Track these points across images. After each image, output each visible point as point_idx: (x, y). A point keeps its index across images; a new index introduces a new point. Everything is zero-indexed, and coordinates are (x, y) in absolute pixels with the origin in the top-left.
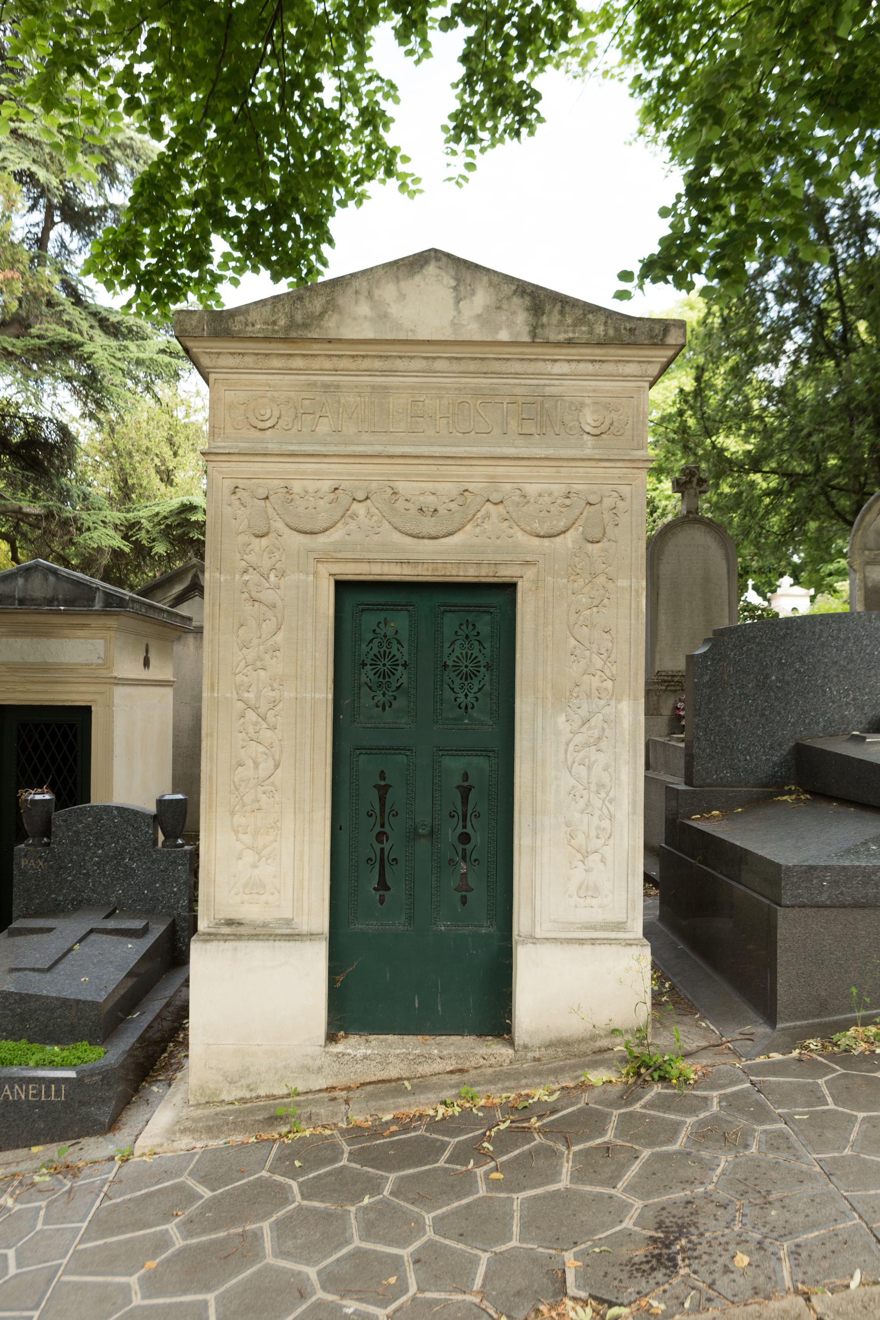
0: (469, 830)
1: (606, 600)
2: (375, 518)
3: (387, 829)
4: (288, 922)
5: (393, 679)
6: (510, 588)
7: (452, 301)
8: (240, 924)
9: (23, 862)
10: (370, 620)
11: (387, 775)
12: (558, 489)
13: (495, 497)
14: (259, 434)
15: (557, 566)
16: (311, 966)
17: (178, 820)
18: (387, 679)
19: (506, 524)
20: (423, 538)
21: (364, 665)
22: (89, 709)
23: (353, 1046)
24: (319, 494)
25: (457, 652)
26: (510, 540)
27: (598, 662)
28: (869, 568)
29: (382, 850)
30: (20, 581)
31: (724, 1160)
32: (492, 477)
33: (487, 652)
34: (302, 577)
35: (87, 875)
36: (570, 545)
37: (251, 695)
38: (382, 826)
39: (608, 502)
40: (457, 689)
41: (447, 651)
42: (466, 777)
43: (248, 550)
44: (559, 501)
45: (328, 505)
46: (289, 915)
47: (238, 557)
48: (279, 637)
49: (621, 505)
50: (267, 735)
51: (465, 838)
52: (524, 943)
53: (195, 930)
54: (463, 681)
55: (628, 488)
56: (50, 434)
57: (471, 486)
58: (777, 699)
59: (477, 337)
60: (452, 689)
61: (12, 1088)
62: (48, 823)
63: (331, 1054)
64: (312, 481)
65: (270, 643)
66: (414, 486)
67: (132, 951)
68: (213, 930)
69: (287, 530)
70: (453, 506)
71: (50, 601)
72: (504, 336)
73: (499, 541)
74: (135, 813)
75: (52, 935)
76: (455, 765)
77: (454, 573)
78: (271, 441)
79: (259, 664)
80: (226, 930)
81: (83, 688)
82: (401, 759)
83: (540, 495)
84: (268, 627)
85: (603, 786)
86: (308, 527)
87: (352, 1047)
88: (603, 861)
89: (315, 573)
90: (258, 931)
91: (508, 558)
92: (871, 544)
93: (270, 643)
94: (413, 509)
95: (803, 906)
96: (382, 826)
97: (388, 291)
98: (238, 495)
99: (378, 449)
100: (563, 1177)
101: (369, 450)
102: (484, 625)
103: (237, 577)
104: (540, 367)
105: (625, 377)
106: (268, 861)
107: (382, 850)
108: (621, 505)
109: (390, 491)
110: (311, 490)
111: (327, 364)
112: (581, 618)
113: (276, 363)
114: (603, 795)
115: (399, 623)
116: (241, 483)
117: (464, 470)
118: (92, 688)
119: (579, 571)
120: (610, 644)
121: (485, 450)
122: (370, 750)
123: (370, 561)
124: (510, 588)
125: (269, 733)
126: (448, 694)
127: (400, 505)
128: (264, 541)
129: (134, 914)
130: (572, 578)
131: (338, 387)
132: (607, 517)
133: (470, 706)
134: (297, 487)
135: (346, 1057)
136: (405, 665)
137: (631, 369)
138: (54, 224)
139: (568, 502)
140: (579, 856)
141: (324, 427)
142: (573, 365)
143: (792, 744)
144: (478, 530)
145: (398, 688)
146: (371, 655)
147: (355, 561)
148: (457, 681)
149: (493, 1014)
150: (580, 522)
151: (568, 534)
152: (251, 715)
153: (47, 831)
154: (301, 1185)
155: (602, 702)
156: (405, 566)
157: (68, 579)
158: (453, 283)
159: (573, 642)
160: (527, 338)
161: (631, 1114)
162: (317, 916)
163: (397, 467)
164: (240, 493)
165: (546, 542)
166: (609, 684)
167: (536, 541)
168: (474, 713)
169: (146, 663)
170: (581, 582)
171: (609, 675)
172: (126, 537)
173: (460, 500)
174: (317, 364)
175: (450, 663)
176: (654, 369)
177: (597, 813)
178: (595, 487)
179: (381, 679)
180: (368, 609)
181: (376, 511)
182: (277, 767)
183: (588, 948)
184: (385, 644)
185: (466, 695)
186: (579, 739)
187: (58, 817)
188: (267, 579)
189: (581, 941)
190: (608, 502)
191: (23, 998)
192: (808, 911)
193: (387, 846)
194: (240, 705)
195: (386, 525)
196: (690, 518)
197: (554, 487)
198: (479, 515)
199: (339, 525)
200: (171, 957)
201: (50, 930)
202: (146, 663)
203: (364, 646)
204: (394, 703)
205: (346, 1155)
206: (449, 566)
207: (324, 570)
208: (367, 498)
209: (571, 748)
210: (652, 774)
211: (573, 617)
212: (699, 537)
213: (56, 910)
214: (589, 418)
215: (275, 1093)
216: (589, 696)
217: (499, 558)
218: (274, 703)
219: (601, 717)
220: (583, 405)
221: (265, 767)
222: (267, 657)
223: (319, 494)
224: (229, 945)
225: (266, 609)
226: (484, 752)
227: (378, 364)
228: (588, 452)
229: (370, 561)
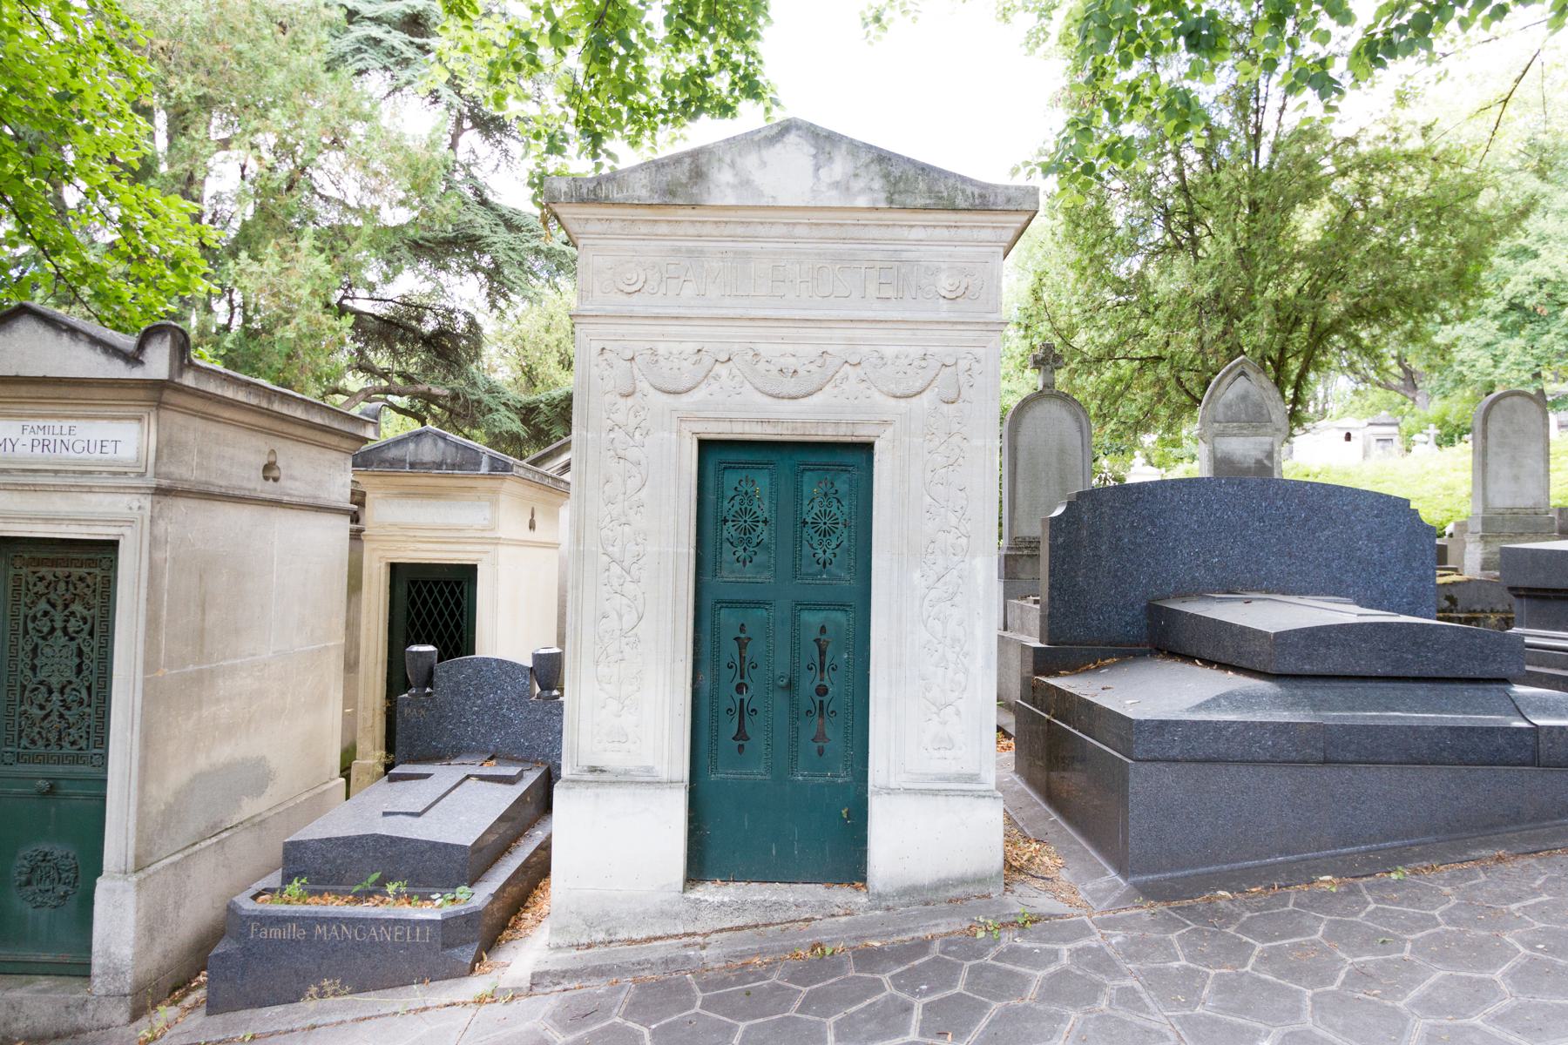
0: (826, 682)
3: (747, 680)
4: (649, 770)
6: (867, 448)
7: (810, 169)
9: (406, 711)
10: (731, 479)
11: (747, 628)
14: (625, 297)
16: (667, 820)
17: (548, 671)
19: (864, 385)
21: (725, 521)
22: (475, 567)
23: (710, 893)
25: (816, 510)
28: (1218, 439)
29: (742, 701)
31: (1074, 1016)
32: (850, 339)
33: (845, 509)
34: (666, 435)
35: (467, 723)
38: (742, 677)
39: (963, 365)
41: (806, 508)
42: (823, 630)
47: (605, 415)
48: (643, 494)
49: (976, 366)
50: (630, 588)
51: (822, 691)
52: (878, 793)
53: (559, 777)
56: (461, 325)
57: (830, 349)
58: (1129, 560)
59: (834, 204)
61: (339, 928)
62: (431, 673)
63: (688, 900)
64: (676, 344)
65: (635, 498)
66: (777, 349)
67: (506, 796)
69: (652, 390)
70: (812, 367)
71: (439, 466)
72: (862, 202)
74: (513, 665)
75: (428, 781)
76: (812, 619)
78: (638, 304)
79: (623, 520)
80: (589, 777)
81: (469, 548)
82: (761, 613)
87: (711, 894)
88: (958, 713)
89: (679, 431)
90: (620, 778)
91: (865, 417)
92: (1220, 417)
93: (635, 498)
94: (774, 371)
95: (1155, 760)
96: (742, 677)
97: (750, 161)
99: (739, 312)
100: (912, 1030)
101: (731, 313)
102: (842, 486)
104: (898, 233)
105: (979, 243)
106: (632, 713)
107: (742, 701)
108: (976, 366)
111: (692, 230)
113: (644, 229)
115: (761, 483)
118: (478, 548)
121: (843, 314)
122: (731, 604)
124: (867, 448)
125: (632, 586)
126: (806, 549)
127: (762, 366)
128: (630, 401)
129: (510, 759)
131: (702, 252)
132: (963, 379)
134: (662, 348)
136: (765, 522)
137: (986, 234)
138: (463, 130)
139: (923, 364)
140: (934, 709)
141: (689, 290)
142: (929, 231)
143: (1144, 604)
144: (836, 391)
146: (732, 512)
147: (717, 420)
148: (816, 537)
149: (848, 861)
150: (935, 383)
151: (924, 395)
152: (615, 569)
153: (429, 680)
154: (654, 1033)
155: (956, 559)
157: (457, 446)
158: (813, 151)
159: (929, 499)
160: (883, 205)
161: (980, 966)
162: (675, 761)
164: (607, 355)
166: (964, 541)
167: (893, 401)
168: (832, 568)
169: (532, 526)
172: (524, 421)
173: (819, 362)
174: (681, 230)
175: (809, 520)
176: (1009, 235)
177: (952, 666)
183: (941, 800)
186: (933, 594)
187: (441, 669)
188: (632, 437)
189: (935, 793)
190: (963, 365)
191: (394, 841)
192: (1160, 765)
193: (746, 696)
195: (748, 385)
196: (1047, 393)
197: (911, 350)
199: (703, 385)
200: (540, 802)
201: (427, 776)
202: (532, 526)
205: (699, 1003)
207: (687, 428)
209: (926, 602)
210: (1007, 634)
212: (1052, 411)
213: (437, 757)
214: (945, 283)
215: (634, 937)
216: (944, 553)
217: (857, 418)
218: (638, 557)
219: (955, 572)
220: (938, 270)
221: (629, 619)
222: (632, 512)
224: (591, 792)
226: (842, 607)
227: (740, 230)
228: (944, 316)
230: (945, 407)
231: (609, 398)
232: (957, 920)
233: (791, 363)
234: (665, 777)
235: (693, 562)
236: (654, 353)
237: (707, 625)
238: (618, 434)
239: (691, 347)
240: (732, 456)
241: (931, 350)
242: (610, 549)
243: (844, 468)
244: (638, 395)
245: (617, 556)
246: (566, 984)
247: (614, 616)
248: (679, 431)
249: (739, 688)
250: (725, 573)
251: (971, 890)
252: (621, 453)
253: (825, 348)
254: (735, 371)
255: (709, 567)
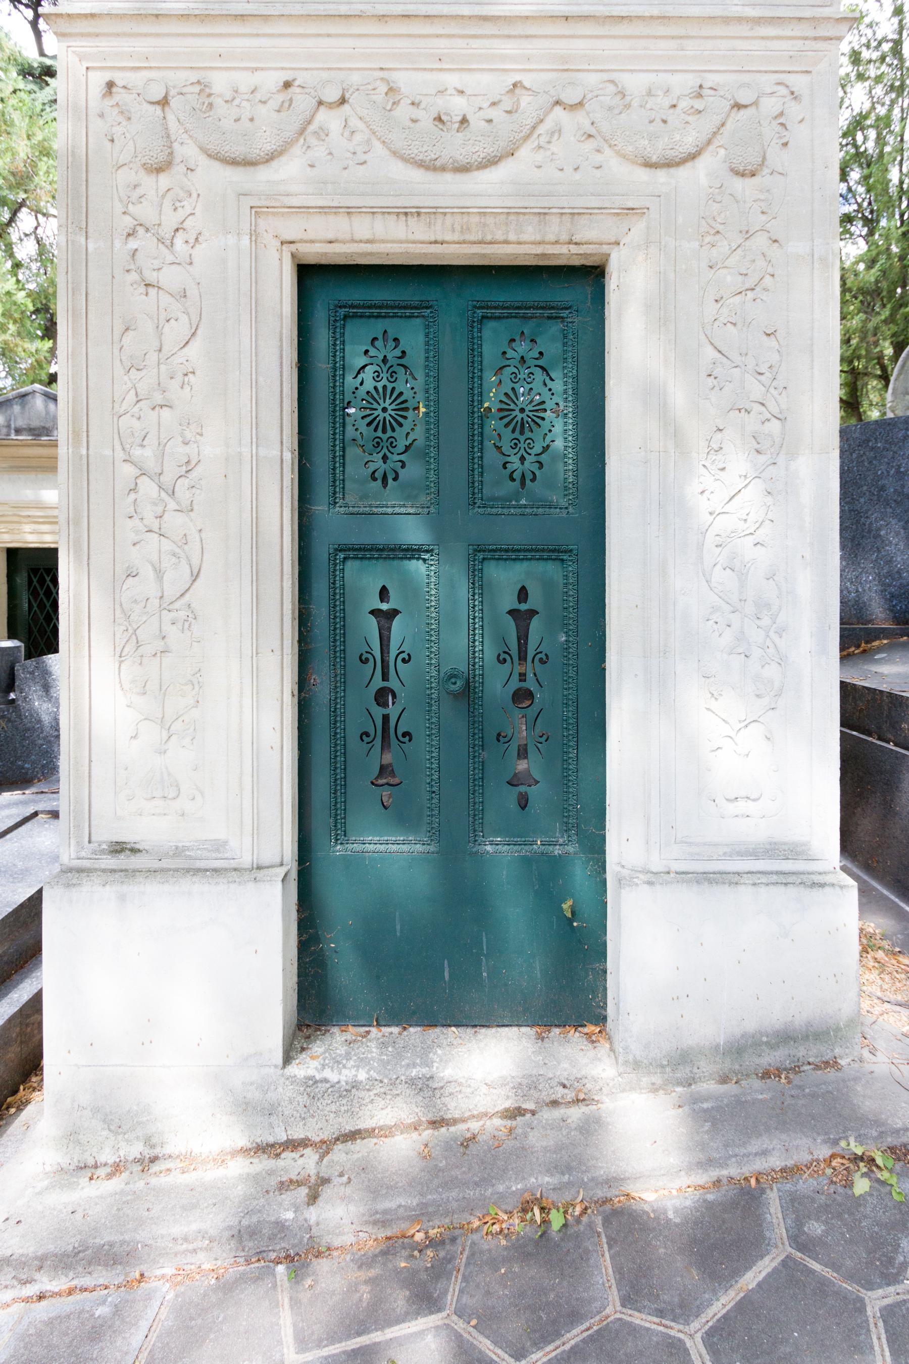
1: (768, 280)
2: (358, 137)
3: (393, 683)
4: (219, 846)
5: (400, 433)
6: (592, 275)
8: (134, 851)
12: (682, 83)
13: (571, 97)
15: (680, 220)
16: (257, 935)
18: (389, 433)
19: (590, 145)
20: (443, 169)
24: (258, 96)
26: (598, 173)
27: (756, 390)
29: (386, 718)
30: (17, 408)
34: (231, 240)
36: (704, 181)
37: (148, 453)
38: (385, 677)
39: (770, 106)
40: (506, 449)
42: (523, 594)
43: (134, 198)
44: (684, 104)
45: (275, 115)
46: (221, 835)
47: (119, 208)
48: (194, 351)
49: (794, 110)
50: (175, 522)
54: (517, 434)
55: (805, 78)
60: (499, 448)
63: (292, 1079)
68: (86, 864)
69: (203, 160)
70: (493, 113)
73: (577, 176)
77: (500, 236)
79: (158, 398)
80: (110, 862)
83: (650, 93)
84: (176, 331)
85: (768, 606)
86: (238, 150)
91: (594, 202)
94: (426, 121)
96: (385, 677)
98: (116, 98)
103: (118, 244)
107: (386, 718)
109: (384, 88)
110: (243, 89)
112: (725, 311)
114: (766, 621)
116: (120, 78)
117: (509, 48)
119: (720, 228)
120: (776, 357)
123: (350, 211)
125: (180, 518)
126: (491, 456)
127: (404, 112)
128: (164, 180)
130: (708, 239)
133: (529, 476)
134: (220, 83)
135: (323, 1086)
139: (699, 104)
144: (539, 157)
145: (407, 448)
148: (507, 434)
152: (148, 487)
156: (412, 221)
159: (711, 353)
163: (397, 43)
164: (120, 95)
165: (661, 175)
166: (775, 425)
167: (643, 174)
170: (724, 247)
171: (775, 411)
173: (507, 104)
178: (746, 78)
179: (379, 433)
180: (355, 316)
181: (360, 125)
182: (195, 577)
184: (384, 375)
185: (522, 459)
193: (393, 710)
194: (129, 471)
195: (377, 145)
198: (541, 129)
199: (297, 150)
203: (349, 378)
204: (402, 473)
206: (490, 220)
208: (343, 101)
211: (711, 309)
217: (580, 202)
221: (176, 578)
222: (175, 384)
223: (258, 96)
225: (171, 300)
226: (554, 553)
229: (350, 211)
230: (738, 184)
231: (125, 177)
232: (804, 1142)
233: (458, 106)
234: (246, 860)
235: (290, 477)
236: (203, 86)
237: (320, 589)
238: (143, 242)
239: (272, 80)
240: (357, 294)
241: (711, 80)
242: (137, 452)
243: (553, 313)
244: (179, 169)
245: (151, 465)
246: (45, 1283)
247: (147, 572)
248: (254, 235)
249: (382, 697)
250: (350, 499)
251: (801, 1052)
252: (151, 277)
253: (517, 77)
254: (354, 122)
255: (322, 489)
